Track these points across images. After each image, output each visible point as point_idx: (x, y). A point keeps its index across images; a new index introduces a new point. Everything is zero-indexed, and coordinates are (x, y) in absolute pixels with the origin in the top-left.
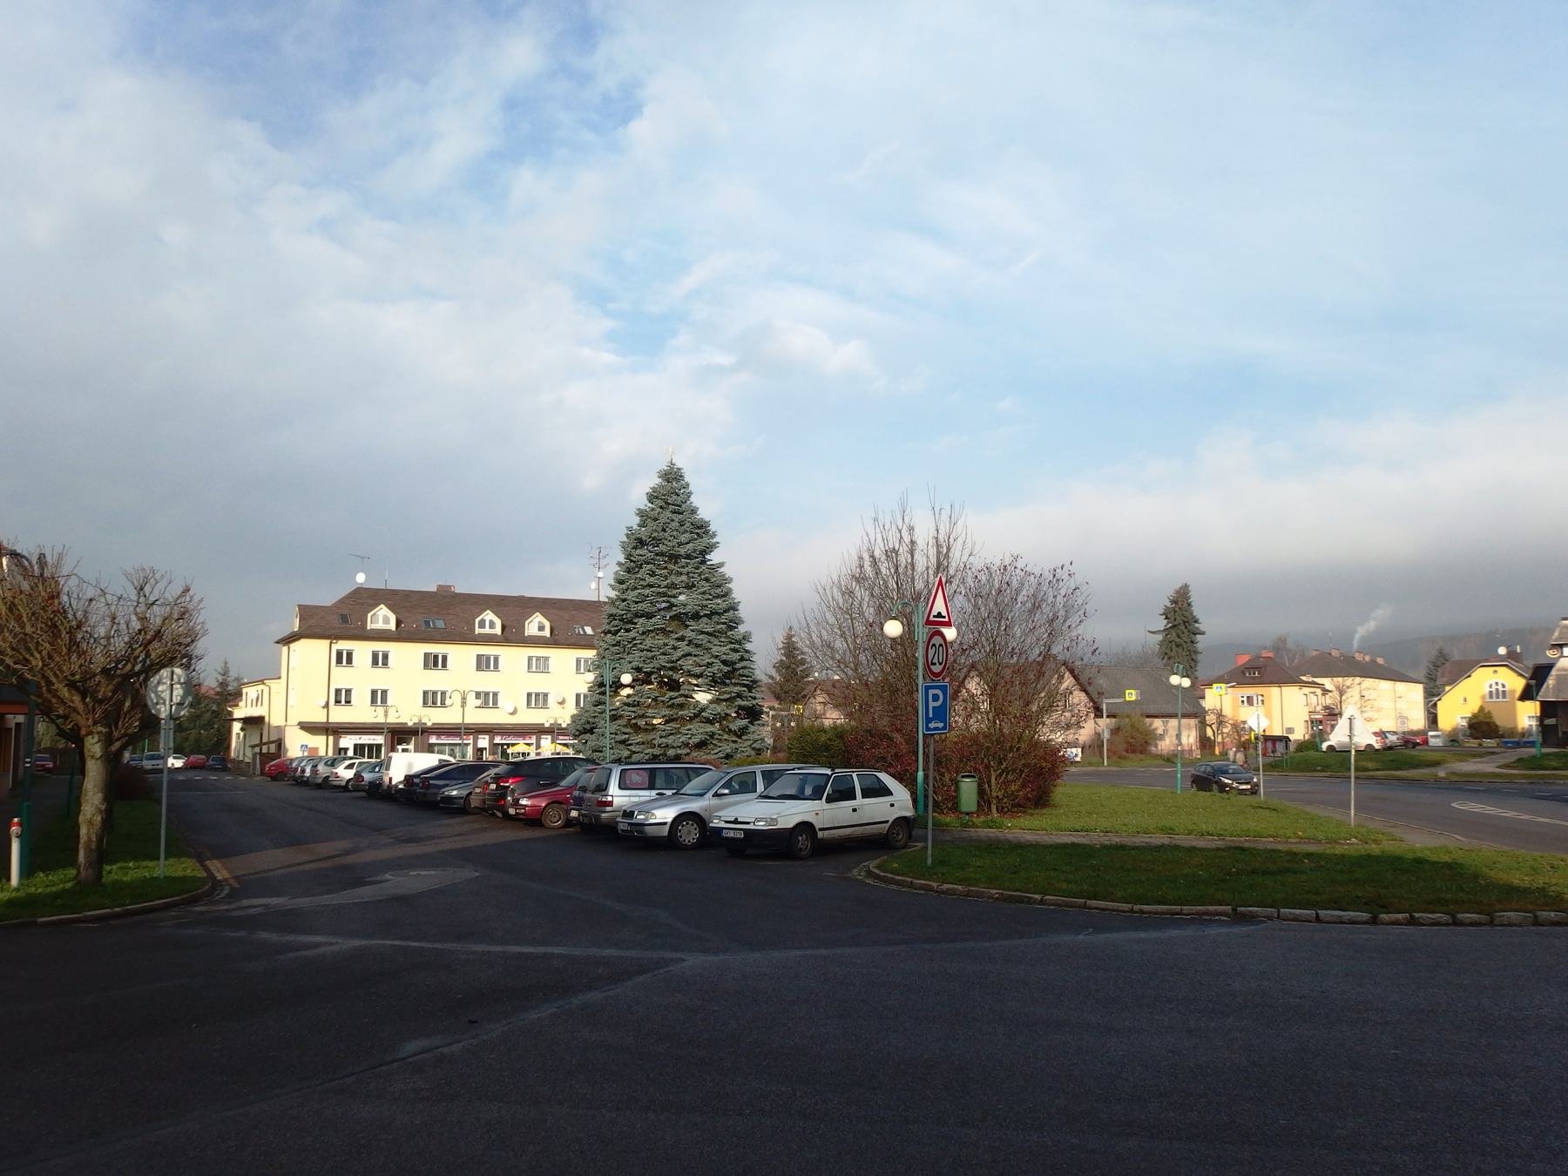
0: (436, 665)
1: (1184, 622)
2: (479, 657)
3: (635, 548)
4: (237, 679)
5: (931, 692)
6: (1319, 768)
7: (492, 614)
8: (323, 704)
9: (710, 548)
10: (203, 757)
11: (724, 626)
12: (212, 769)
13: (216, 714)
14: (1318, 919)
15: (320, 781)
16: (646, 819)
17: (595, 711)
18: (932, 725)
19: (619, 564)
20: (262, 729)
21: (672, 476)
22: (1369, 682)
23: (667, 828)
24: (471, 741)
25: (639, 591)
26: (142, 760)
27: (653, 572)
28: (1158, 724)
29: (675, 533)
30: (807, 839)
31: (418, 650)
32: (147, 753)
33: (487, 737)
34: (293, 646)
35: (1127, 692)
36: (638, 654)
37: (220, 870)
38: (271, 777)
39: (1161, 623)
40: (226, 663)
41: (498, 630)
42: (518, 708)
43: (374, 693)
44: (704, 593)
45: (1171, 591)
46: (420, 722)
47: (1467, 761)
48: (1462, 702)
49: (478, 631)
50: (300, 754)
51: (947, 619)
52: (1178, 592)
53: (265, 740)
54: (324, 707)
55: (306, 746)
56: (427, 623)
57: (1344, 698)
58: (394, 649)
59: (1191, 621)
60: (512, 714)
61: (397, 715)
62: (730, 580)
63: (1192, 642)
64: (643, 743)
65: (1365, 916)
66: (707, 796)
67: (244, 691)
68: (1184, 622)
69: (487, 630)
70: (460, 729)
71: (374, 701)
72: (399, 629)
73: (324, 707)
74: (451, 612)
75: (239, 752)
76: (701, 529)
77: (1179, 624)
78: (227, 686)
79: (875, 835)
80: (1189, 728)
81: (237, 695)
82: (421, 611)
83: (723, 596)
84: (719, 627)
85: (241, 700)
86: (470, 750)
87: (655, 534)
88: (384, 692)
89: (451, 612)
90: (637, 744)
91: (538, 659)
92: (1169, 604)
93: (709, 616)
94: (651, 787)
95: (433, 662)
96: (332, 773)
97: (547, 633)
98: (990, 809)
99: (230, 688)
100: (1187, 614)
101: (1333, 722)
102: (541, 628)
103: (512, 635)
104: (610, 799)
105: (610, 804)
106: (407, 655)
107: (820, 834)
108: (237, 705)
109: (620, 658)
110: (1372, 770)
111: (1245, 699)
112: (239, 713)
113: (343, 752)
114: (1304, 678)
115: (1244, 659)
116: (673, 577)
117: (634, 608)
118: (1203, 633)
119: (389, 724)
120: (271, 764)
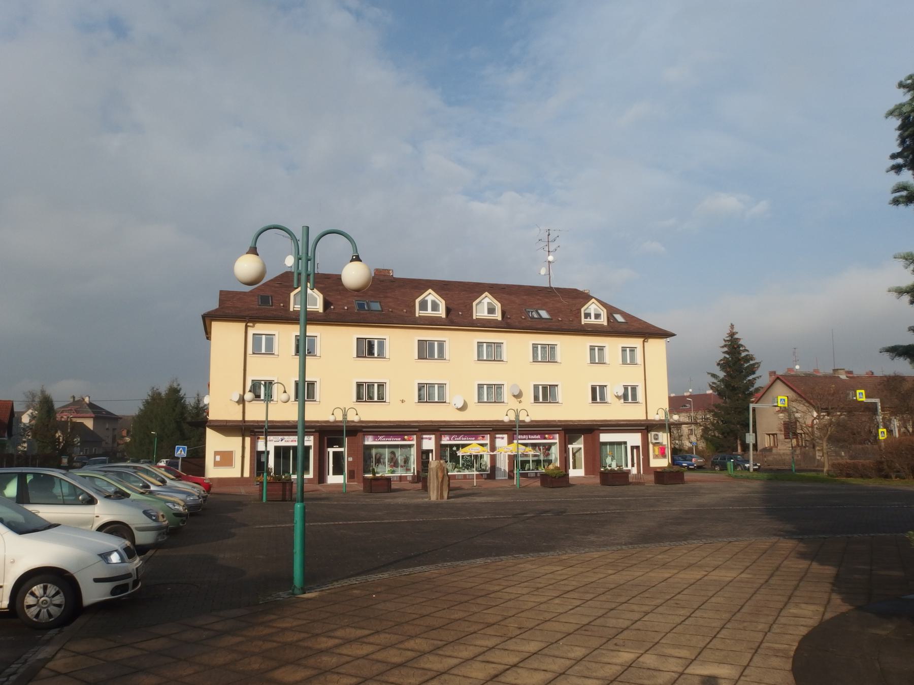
24: (414, 442)
31: (349, 336)
33: (433, 437)
35: (858, 391)
41: (442, 313)
43: (594, 389)
49: (418, 313)
56: (361, 306)
69: (429, 312)
86: (414, 451)
91: (544, 346)
95: (367, 349)
102: (491, 310)
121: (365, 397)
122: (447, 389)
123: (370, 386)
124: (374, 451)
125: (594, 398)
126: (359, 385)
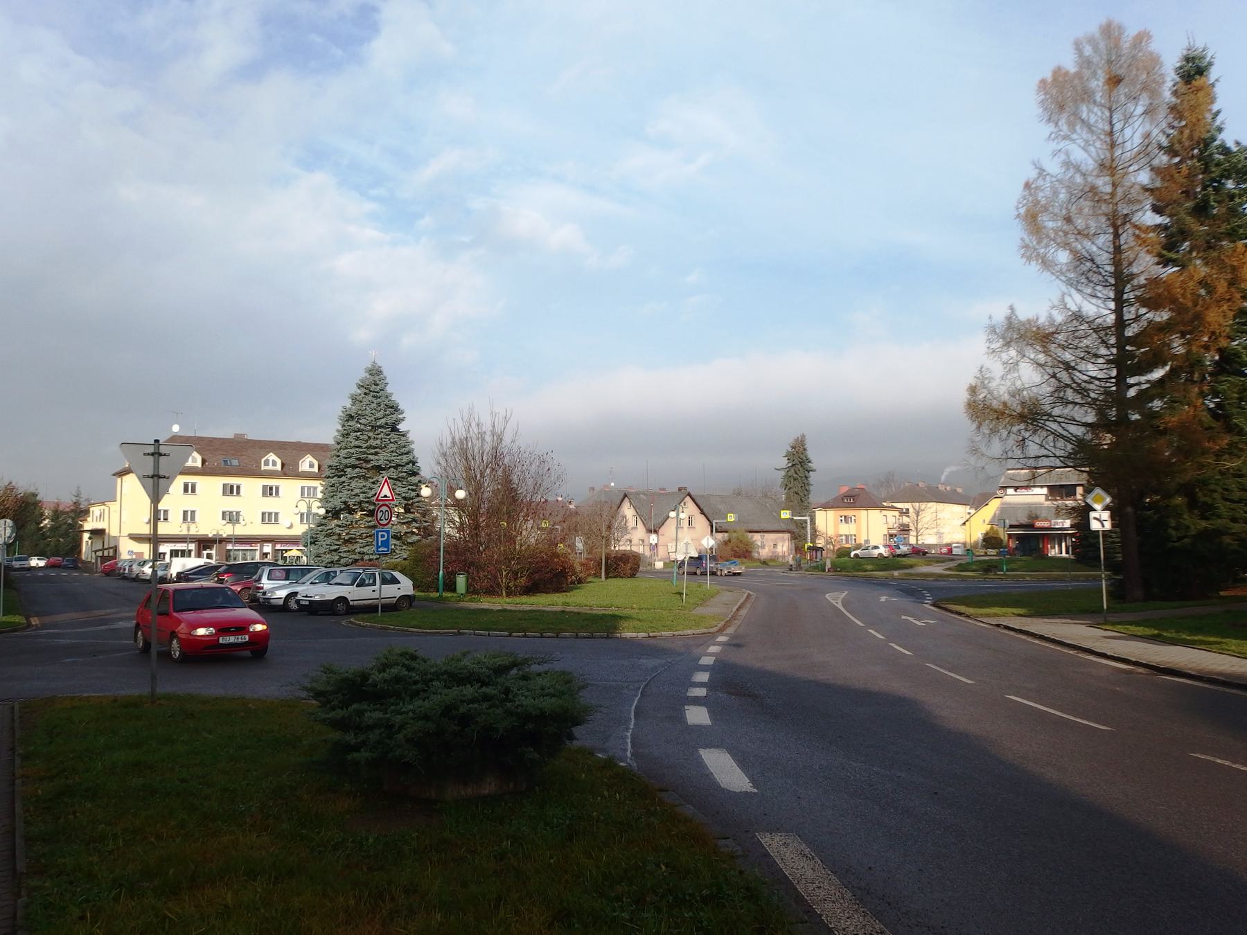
0: (232, 492)
1: (800, 462)
2: (264, 487)
3: (347, 421)
4: (88, 500)
5: (380, 533)
6: (839, 569)
7: (275, 456)
8: (147, 520)
9: (399, 421)
10: (60, 558)
11: (405, 474)
12: (65, 568)
13: (71, 526)
14: (489, 635)
15: (134, 576)
16: (271, 596)
17: (317, 530)
18: (380, 549)
19: (338, 431)
20: (103, 538)
21: (375, 372)
22: (933, 506)
23: (283, 600)
24: (258, 548)
25: (347, 450)
26: (12, 561)
27: (358, 438)
28: (757, 537)
29: (373, 412)
30: (343, 605)
31: (218, 482)
32: (17, 556)
33: (270, 545)
34: (124, 478)
35: (729, 515)
36: (346, 492)
37: (35, 621)
38: (106, 574)
39: (784, 463)
40: (78, 487)
41: (279, 467)
42: (293, 523)
43: (185, 513)
44: (392, 452)
45: (791, 441)
46: (218, 534)
47: (931, 565)
48: (982, 522)
49: (263, 468)
50: (129, 557)
51: (391, 498)
52: (797, 440)
53: (106, 546)
54: (147, 523)
55: (132, 552)
56: (225, 462)
57: (919, 518)
58: (201, 482)
59: (806, 462)
60: (288, 528)
61: (197, 530)
62: (412, 442)
63: (806, 477)
64: (349, 551)
65: (538, 634)
66: (306, 584)
67: (91, 509)
68: (800, 462)
69: (270, 467)
70: (231, 539)
71: (185, 518)
72: (204, 466)
73: (147, 523)
74: (244, 453)
75: (88, 556)
76: (395, 408)
77: (797, 464)
78: (80, 504)
79: (387, 604)
80: (783, 540)
81: (86, 512)
82: (221, 452)
83: (405, 454)
84: (401, 475)
85: (89, 516)
86: (258, 553)
87: (360, 412)
88: (193, 512)
89: (244, 453)
90: (344, 552)
91: (309, 488)
92: (790, 449)
93: (396, 467)
94: (287, 579)
95: (230, 490)
96: (140, 571)
97: (316, 469)
98: (502, 593)
99: (82, 506)
100: (802, 456)
101: (905, 536)
102: (311, 466)
103: (289, 471)
104: (262, 585)
105: (262, 588)
106: (210, 486)
107: (351, 603)
108: (86, 520)
109: (334, 495)
110: (870, 571)
111: (843, 518)
112: (89, 525)
113: (162, 556)
114: (885, 504)
115: (844, 490)
116: (371, 441)
117: (344, 461)
118: (815, 471)
119: (191, 535)
120: (106, 564)
121: (267, 521)
122: (169, 512)
123: (270, 514)
124: (232, 553)
125: (263, 520)
126: (263, 514)
